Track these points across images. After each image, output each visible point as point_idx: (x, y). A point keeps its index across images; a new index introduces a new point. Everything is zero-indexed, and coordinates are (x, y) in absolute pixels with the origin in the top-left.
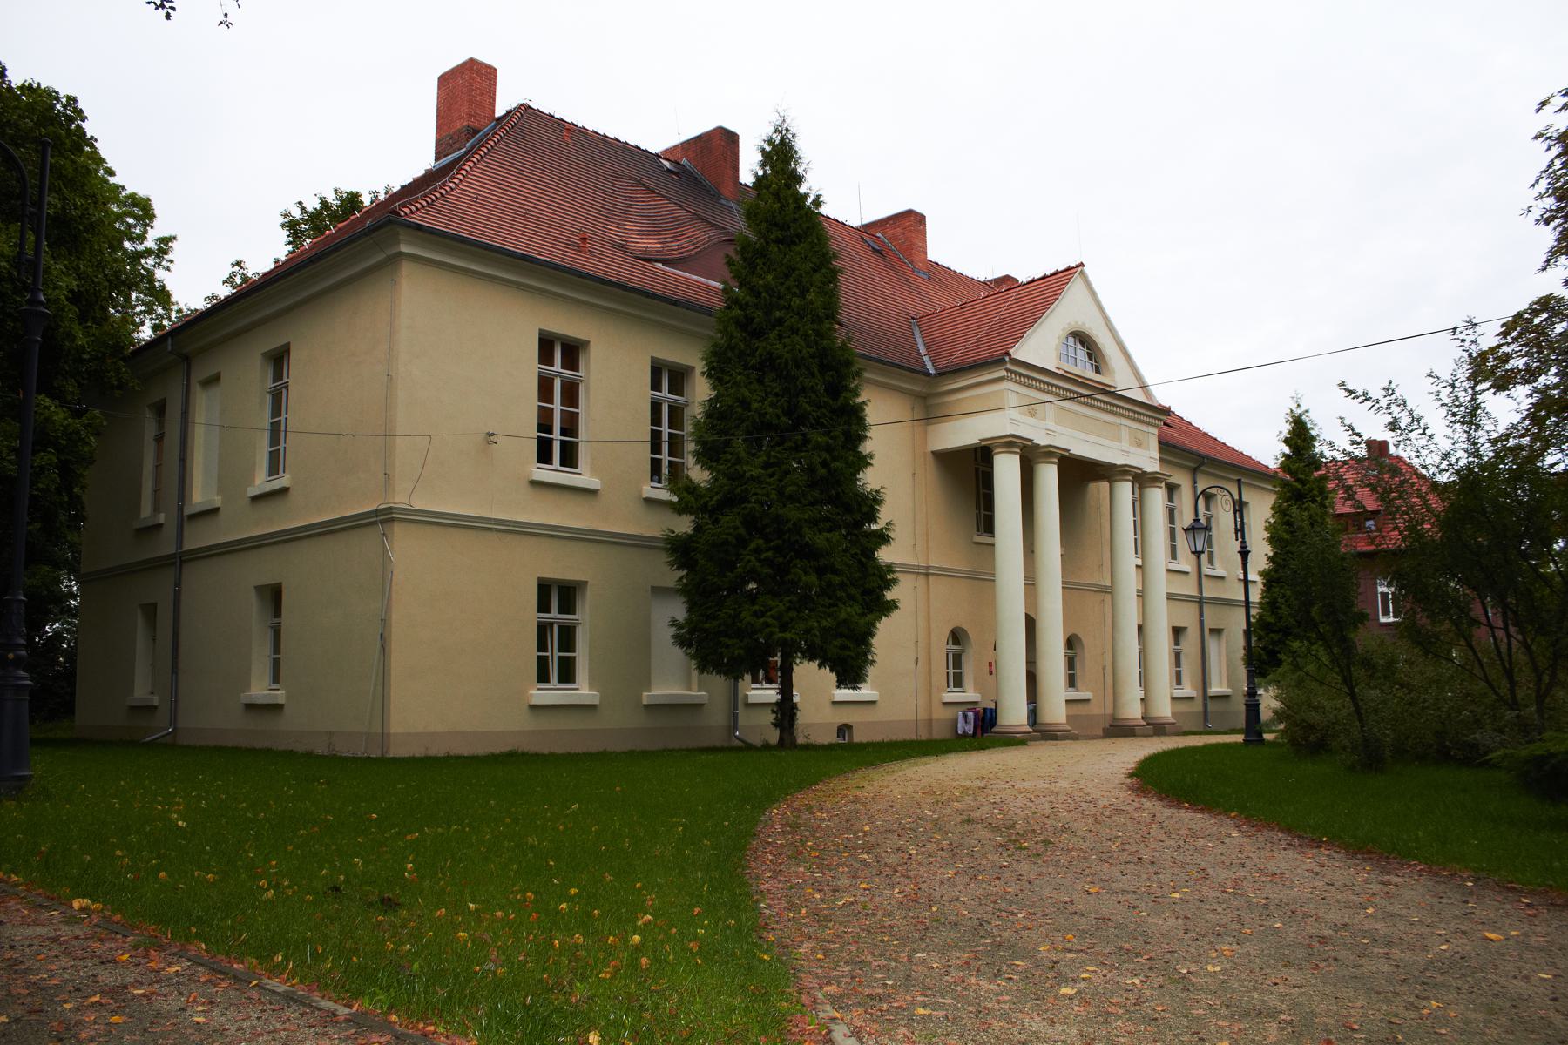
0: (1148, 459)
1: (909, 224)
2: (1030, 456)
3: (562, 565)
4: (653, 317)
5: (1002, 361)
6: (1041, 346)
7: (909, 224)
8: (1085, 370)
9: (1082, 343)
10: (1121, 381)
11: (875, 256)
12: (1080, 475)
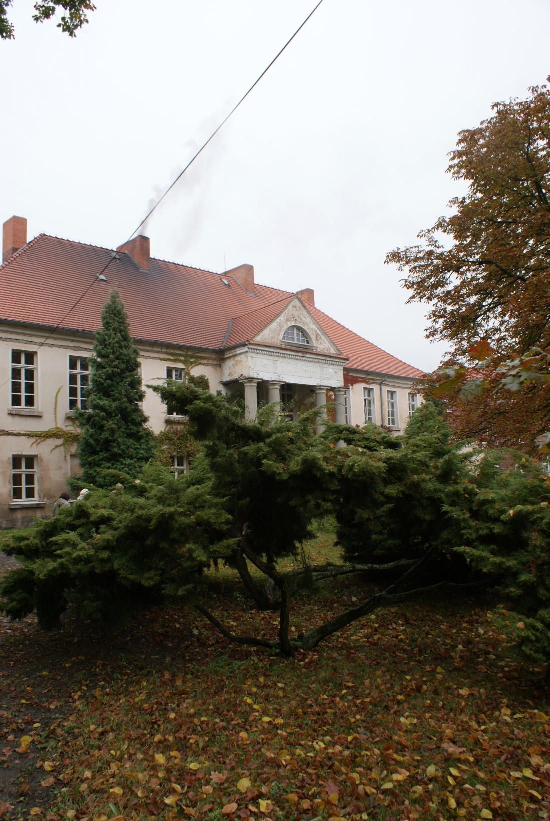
2: (263, 387)
3: (26, 447)
7: (248, 270)
8: (297, 339)
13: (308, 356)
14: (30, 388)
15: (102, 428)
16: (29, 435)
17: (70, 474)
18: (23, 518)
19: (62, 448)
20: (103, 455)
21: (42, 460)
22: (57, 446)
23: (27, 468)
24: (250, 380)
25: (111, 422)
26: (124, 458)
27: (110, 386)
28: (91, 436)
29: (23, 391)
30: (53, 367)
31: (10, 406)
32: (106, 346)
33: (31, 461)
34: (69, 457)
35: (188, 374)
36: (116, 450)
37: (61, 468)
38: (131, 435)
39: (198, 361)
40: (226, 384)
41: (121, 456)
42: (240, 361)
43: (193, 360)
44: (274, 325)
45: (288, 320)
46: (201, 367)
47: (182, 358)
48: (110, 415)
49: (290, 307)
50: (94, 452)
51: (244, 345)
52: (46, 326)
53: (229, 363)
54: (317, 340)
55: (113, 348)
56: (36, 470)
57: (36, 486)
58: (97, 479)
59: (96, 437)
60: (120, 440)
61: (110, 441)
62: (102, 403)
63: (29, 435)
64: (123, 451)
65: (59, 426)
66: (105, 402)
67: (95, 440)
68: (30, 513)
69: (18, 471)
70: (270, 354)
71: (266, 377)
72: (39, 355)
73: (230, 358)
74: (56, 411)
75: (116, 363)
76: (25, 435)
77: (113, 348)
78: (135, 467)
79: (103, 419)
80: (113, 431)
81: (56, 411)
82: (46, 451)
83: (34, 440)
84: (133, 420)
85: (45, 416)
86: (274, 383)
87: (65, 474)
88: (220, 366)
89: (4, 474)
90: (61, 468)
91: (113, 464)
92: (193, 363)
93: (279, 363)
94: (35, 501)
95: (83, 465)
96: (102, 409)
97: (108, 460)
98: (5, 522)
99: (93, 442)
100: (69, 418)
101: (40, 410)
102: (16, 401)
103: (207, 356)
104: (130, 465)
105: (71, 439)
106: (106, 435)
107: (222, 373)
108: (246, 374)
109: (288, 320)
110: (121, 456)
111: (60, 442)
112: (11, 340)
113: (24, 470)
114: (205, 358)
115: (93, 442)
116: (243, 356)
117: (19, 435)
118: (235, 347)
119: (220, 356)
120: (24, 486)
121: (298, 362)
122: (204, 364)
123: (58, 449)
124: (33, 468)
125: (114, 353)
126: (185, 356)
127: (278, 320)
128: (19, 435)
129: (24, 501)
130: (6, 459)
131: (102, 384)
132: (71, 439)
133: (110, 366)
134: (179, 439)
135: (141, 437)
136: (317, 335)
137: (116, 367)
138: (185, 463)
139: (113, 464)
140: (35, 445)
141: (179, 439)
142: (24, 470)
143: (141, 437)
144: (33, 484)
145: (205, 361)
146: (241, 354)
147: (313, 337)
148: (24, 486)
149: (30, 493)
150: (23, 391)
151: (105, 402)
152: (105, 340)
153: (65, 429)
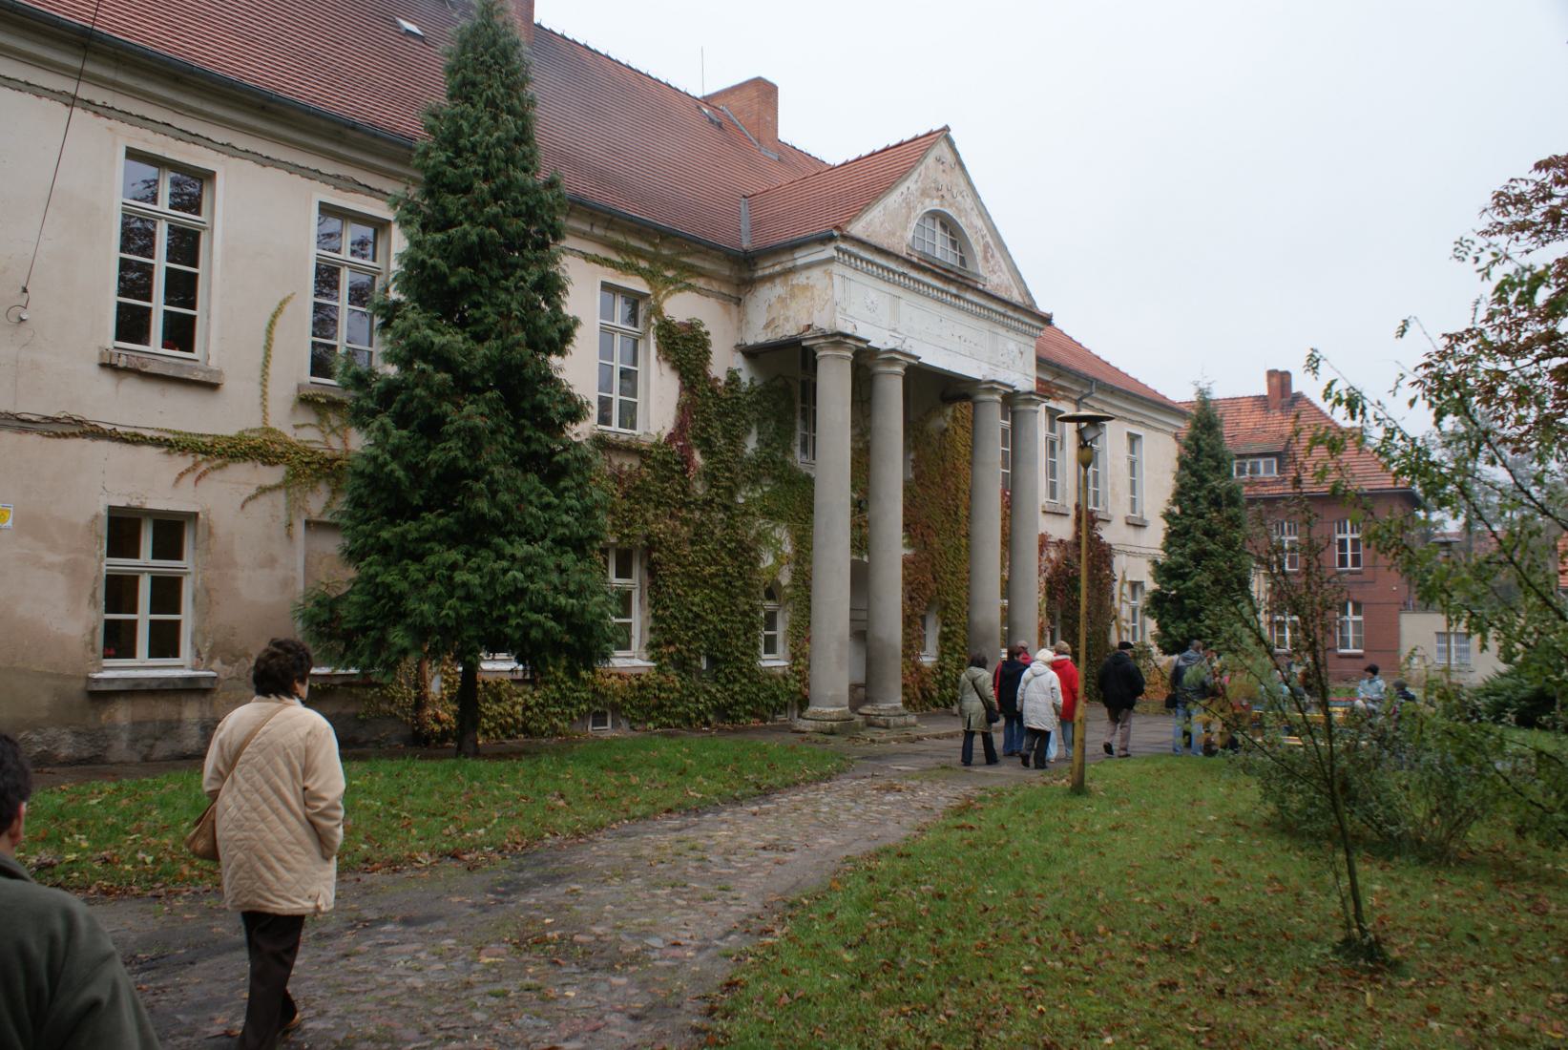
0: (1023, 377)
1: (763, 92)
2: (865, 364)
3: (155, 484)
4: (195, 103)
5: (831, 238)
6: (889, 220)
7: (763, 92)
8: (941, 251)
9: (944, 226)
10: (995, 280)
11: (714, 129)
12: (937, 393)
13: (969, 296)
14: (183, 289)
15: (432, 428)
16: (171, 444)
17: (301, 587)
18: (137, 724)
19: (280, 498)
20: (432, 521)
21: (210, 533)
22: (263, 490)
23: (154, 653)
24: (838, 339)
25: (468, 409)
26: (505, 536)
27: (467, 288)
28: (396, 453)
29: (158, 295)
30: (271, 233)
31: (109, 340)
32: (459, 152)
33: (171, 532)
34: (299, 529)
35: (657, 311)
36: (483, 505)
37: (271, 562)
38: (529, 461)
39: (684, 277)
40: (751, 353)
41: (496, 527)
42: (806, 288)
43: (669, 274)
44: (893, 200)
45: (924, 193)
46: (688, 295)
47: (643, 264)
48: (465, 385)
49: (930, 160)
50: (400, 511)
51: (826, 239)
52: (249, 90)
53: (768, 295)
54: (986, 259)
55: (485, 160)
56: (189, 565)
57: (187, 618)
58: (411, 604)
59: (409, 457)
60: (498, 472)
61: (463, 474)
62: (438, 340)
63: (171, 444)
64: (505, 509)
65: (272, 424)
66: (452, 339)
67: (409, 468)
68: (162, 709)
69: (123, 565)
70: (886, 276)
71: (880, 339)
72: (220, 181)
73: (771, 278)
74: (265, 374)
75: (493, 209)
76: (157, 443)
77: (485, 160)
78: (545, 569)
79: (441, 395)
80: (473, 440)
81: (265, 374)
82: (222, 499)
83: (186, 462)
84: (539, 408)
85: (228, 385)
86: (891, 357)
87: (286, 583)
88: (738, 302)
89: (73, 569)
90: (271, 562)
91: (468, 556)
92: (668, 281)
93: (902, 302)
94: (179, 668)
95: (353, 556)
96: (442, 360)
97: (452, 539)
98: (69, 739)
99: (400, 473)
100: (306, 401)
101: (213, 363)
102: (131, 325)
103: (707, 265)
104: (528, 560)
105: (312, 469)
106: (450, 450)
107: (742, 322)
108: (823, 321)
109: (924, 193)
110: (496, 527)
111: (274, 475)
112: (125, 116)
113: (145, 562)
114: (700, 273)
115: (400, 473)
116: (816, 274)
117: (135, 440)
118: (794, 247)
119: (743, 270)
120: (144, 617)
121: (945, 311)
122: (698, 291)
123: (265, 500)
124: (178, 555)
125: (487, 177)
126: (652, 259)
127: (903, 188)
128: (135, 440)
129: (142, 667)
130: (83, 519)
131: (444, 278)
132: (312, 469)
133: (471, 218)
134: (626, 496)
135: (562, 470)
136: (986, 246)
137: (493, 222)
138: (636, 570)
139: (468, 556)
140: (190, 478)
141: (626, 496)
142: (145, 562)
143: (562, 470)
144: (176, 609)
145: (701, 283)
146: (809, 266)
147: (978, 249)
148: (144, 617)
149: (165, 642)
150: (158, 295)
151: (452, 339)
152: (459, 132)
153: (291, 435)
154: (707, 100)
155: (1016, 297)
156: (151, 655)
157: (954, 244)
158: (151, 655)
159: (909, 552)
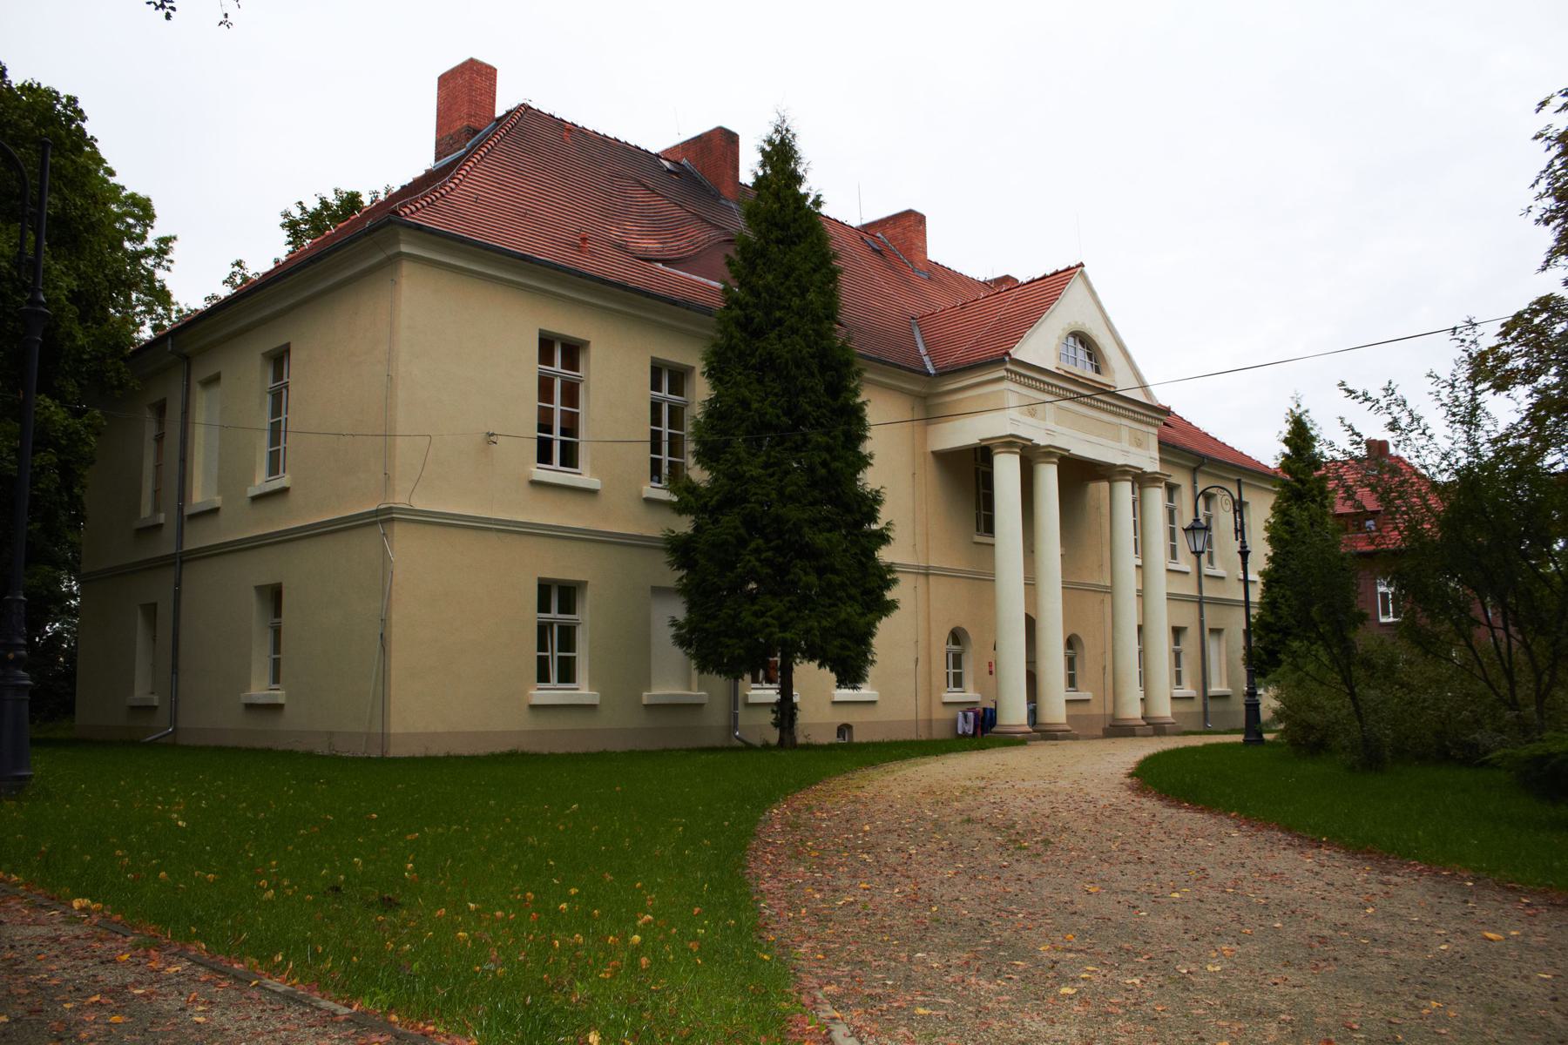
0: (1148, 459)
1: (909, 224)
2: (1030, 456)
3: (562, 565)
6: (1041, 346)
7: (909, 224)
8: (1085, 371)
9: (1082, 343)
10: (1120, 380)
12: (1080, 475)
14: (570, 428)
149: (567, 675)
154: (868, 228)
155: (1138, 395)
156: (560, 681)
157: (1090, 356)
158: (560, 681)
159: (366, 200)
